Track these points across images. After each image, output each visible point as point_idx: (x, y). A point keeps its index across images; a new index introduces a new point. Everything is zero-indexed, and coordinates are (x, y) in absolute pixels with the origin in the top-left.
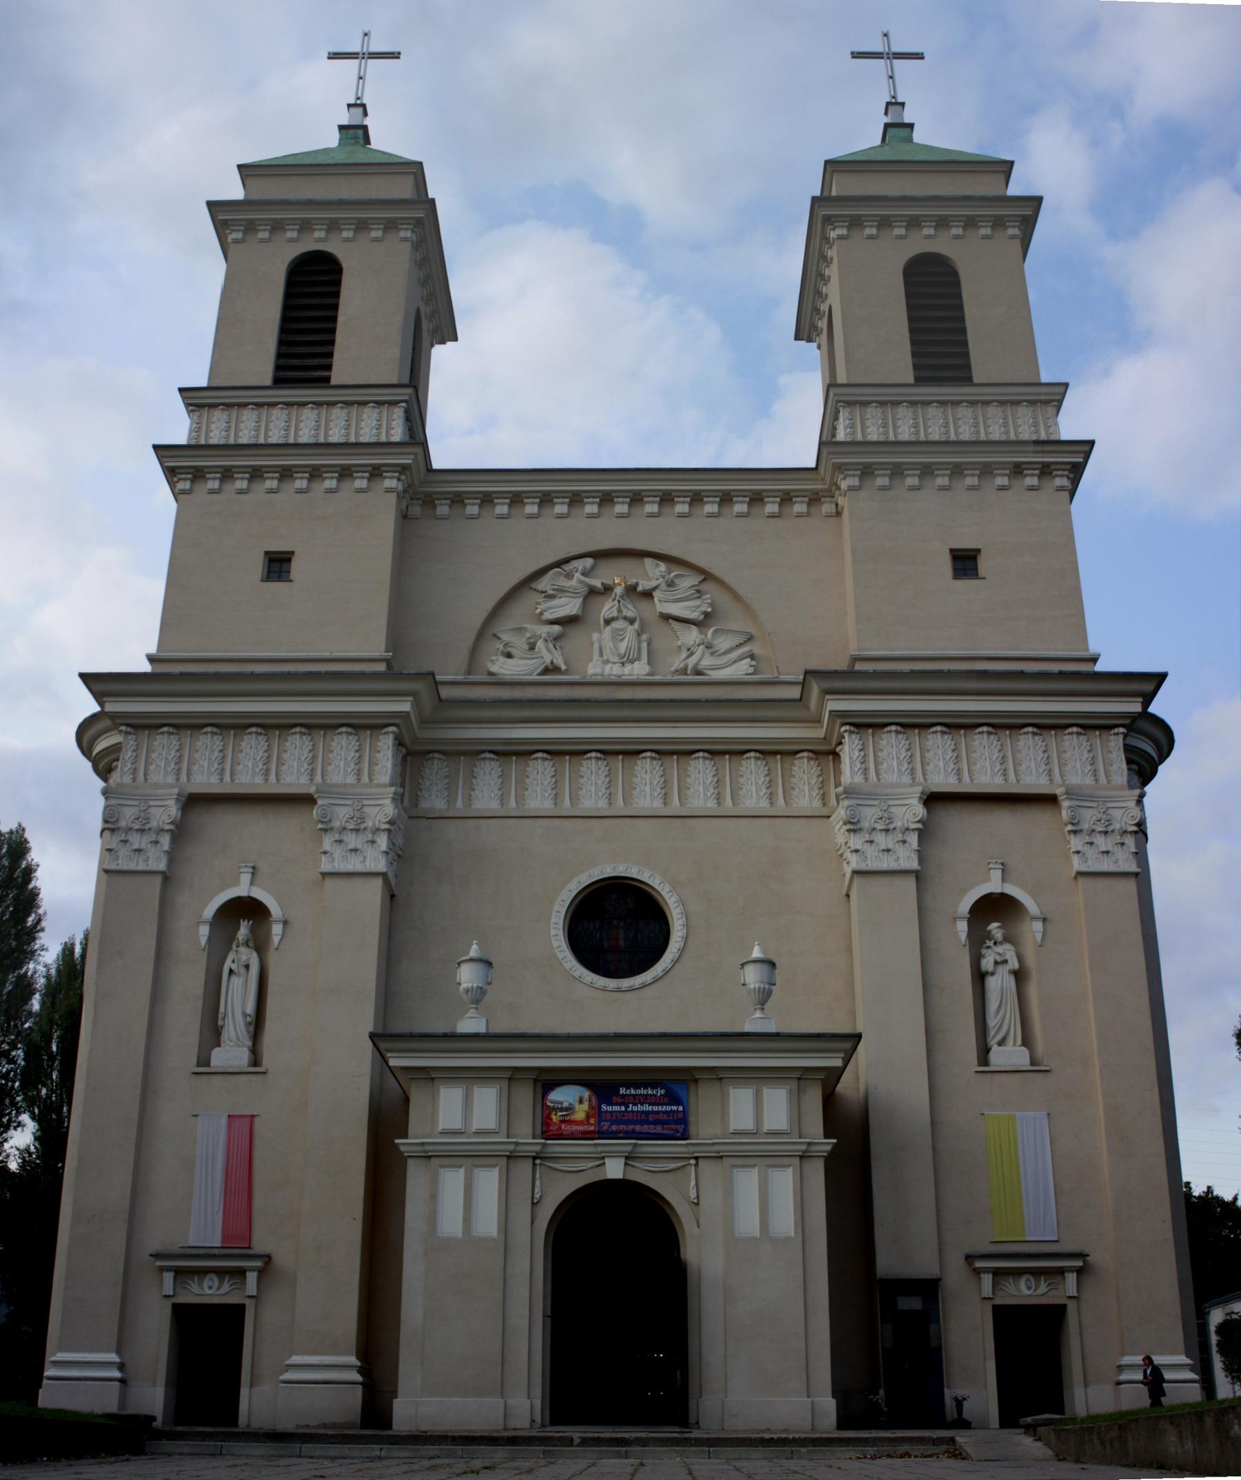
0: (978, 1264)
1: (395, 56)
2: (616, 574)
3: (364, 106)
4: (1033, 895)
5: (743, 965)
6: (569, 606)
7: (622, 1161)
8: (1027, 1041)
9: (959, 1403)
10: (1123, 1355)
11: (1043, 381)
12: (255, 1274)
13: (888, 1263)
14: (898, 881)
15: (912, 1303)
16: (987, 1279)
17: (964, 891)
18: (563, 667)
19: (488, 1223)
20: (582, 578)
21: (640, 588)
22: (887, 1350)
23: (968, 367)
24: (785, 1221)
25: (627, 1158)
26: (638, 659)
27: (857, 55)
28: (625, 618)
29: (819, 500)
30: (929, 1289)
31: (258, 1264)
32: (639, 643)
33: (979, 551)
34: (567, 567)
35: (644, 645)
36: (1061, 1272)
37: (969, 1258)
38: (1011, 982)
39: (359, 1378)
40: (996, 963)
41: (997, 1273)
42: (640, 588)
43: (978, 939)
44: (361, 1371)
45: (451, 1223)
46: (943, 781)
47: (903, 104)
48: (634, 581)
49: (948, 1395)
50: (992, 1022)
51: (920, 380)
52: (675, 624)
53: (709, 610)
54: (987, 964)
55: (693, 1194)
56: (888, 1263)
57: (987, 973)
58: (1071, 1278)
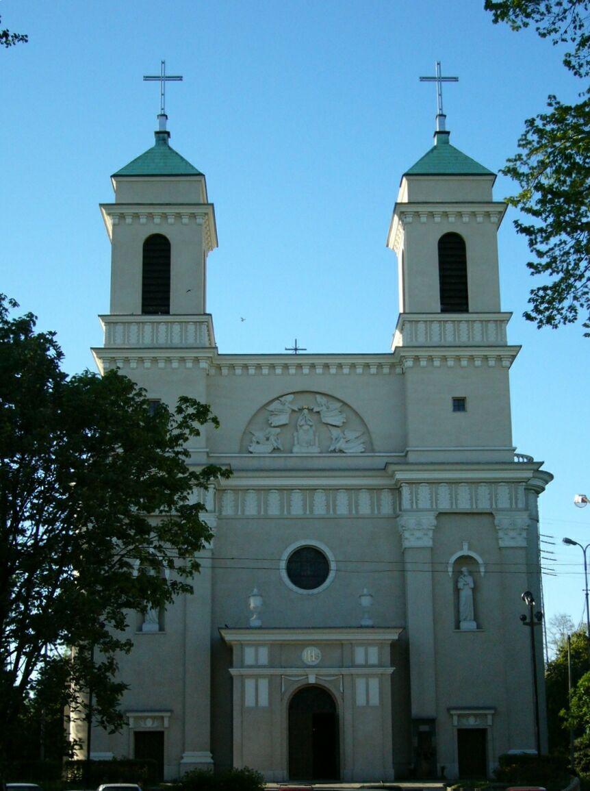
0: (453, 712)
1: (180, 78)
2: (305, 401)
3: (166, 116)
4: (481, 555)
5: (360, 596)
6: (283, 419)
7: (315, 676)
8: (476, 619)
9: (443, 768)
10: (510, 749)
11: (502, 311)
12: (167, 719)
13: (416, 710)
14: (472, 311)
15: (424, 728)
16: (455, 718)
17: (452, 554)
18: (282, 449)
19: (264, 700)
20: (290, 406)
21: (315, 410)
22: (415, 746)
23: (467, 304)
24: (375, 700)
25: (317, 675)
26: (314, 445)
27: (423, 79)
28: (309, 425)
29: (395, 366)
30: (431, 721)
31: (493, 712)
32: (315, 439)
33: (465, 398)
34: (282, 399)
35: (317, 439)
36: (486, 715)
37: (449, 710)
38: (470, 593)
39: (212, 761)
40: (464, 584)
41: (459, 716)
42: (315, 410)
43: (458, 574)
44: (212, 758)
45: (250, 701)
46: (444, 505)
47: (445, 116)
48: (312, 407)
49: (438, 765)
50: (462, 609)
51: (443, 311)
52: (330, 428)
53: (345, 421)
54: (460, 585)
55: (341, 689)
56: (416, 710)
57: (460, 589)
58: (490, 717)
